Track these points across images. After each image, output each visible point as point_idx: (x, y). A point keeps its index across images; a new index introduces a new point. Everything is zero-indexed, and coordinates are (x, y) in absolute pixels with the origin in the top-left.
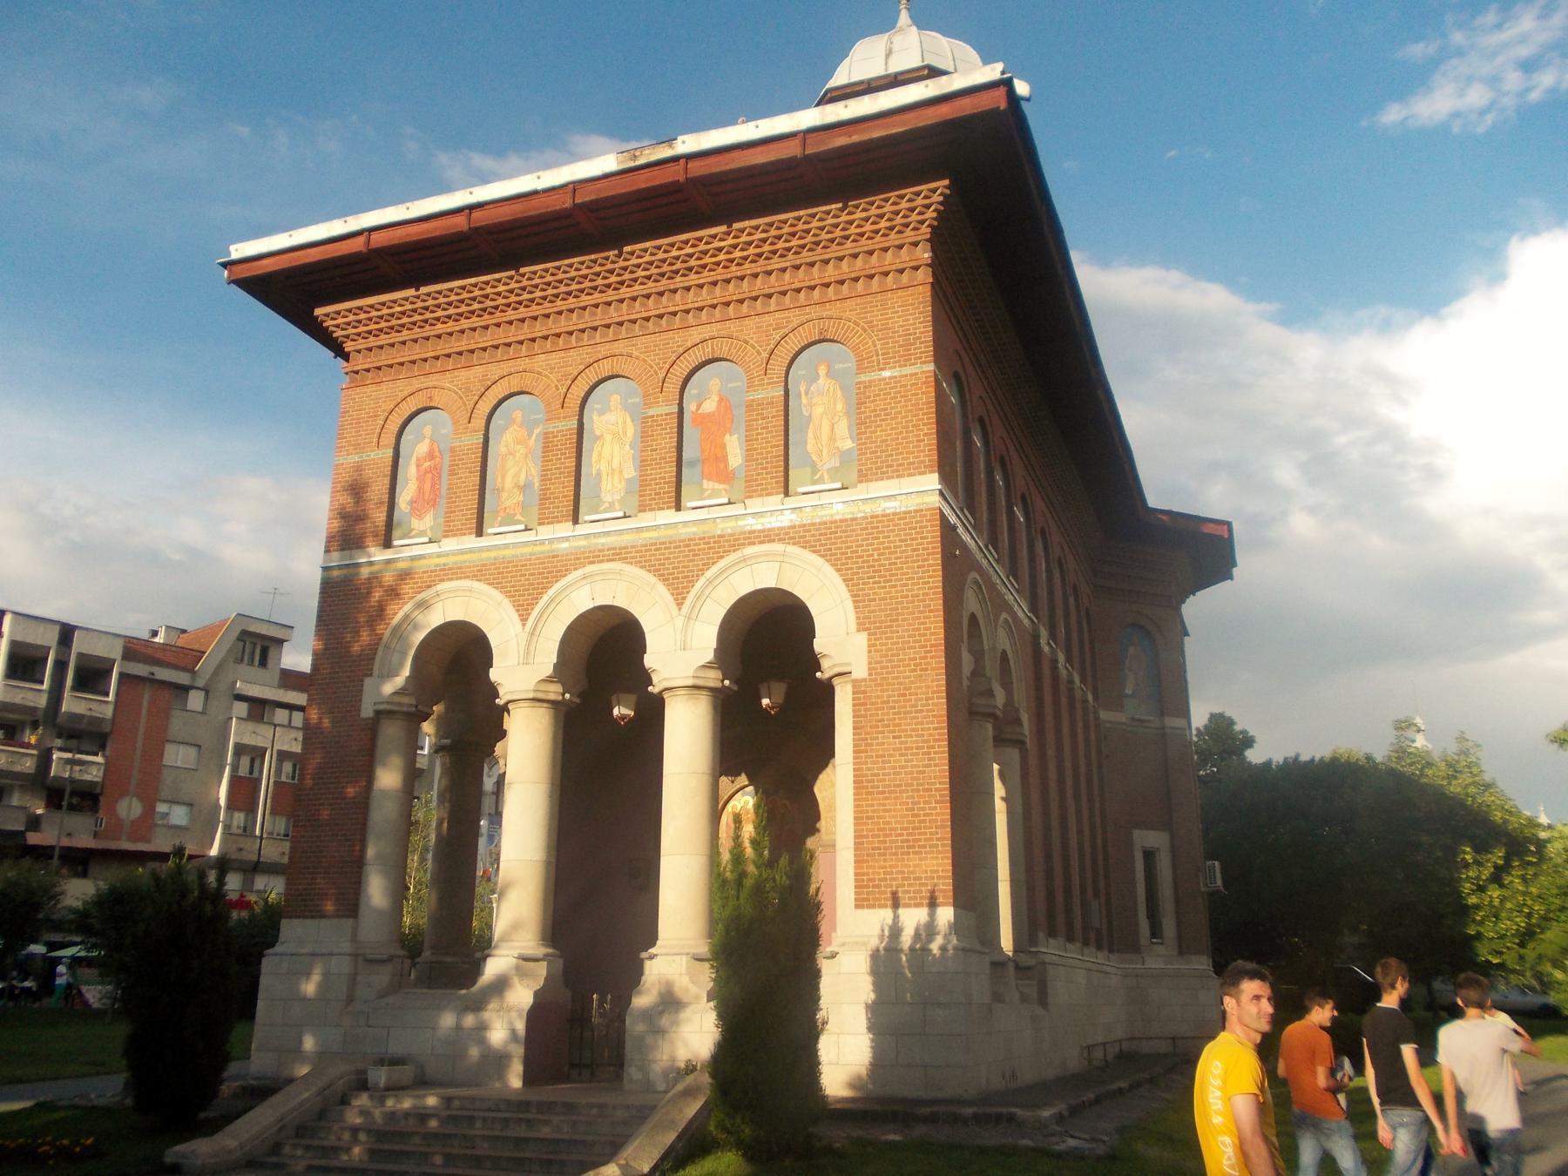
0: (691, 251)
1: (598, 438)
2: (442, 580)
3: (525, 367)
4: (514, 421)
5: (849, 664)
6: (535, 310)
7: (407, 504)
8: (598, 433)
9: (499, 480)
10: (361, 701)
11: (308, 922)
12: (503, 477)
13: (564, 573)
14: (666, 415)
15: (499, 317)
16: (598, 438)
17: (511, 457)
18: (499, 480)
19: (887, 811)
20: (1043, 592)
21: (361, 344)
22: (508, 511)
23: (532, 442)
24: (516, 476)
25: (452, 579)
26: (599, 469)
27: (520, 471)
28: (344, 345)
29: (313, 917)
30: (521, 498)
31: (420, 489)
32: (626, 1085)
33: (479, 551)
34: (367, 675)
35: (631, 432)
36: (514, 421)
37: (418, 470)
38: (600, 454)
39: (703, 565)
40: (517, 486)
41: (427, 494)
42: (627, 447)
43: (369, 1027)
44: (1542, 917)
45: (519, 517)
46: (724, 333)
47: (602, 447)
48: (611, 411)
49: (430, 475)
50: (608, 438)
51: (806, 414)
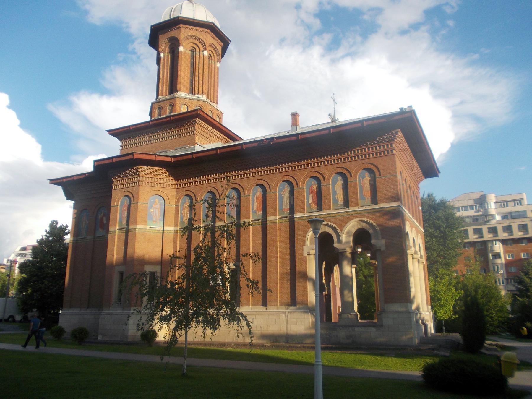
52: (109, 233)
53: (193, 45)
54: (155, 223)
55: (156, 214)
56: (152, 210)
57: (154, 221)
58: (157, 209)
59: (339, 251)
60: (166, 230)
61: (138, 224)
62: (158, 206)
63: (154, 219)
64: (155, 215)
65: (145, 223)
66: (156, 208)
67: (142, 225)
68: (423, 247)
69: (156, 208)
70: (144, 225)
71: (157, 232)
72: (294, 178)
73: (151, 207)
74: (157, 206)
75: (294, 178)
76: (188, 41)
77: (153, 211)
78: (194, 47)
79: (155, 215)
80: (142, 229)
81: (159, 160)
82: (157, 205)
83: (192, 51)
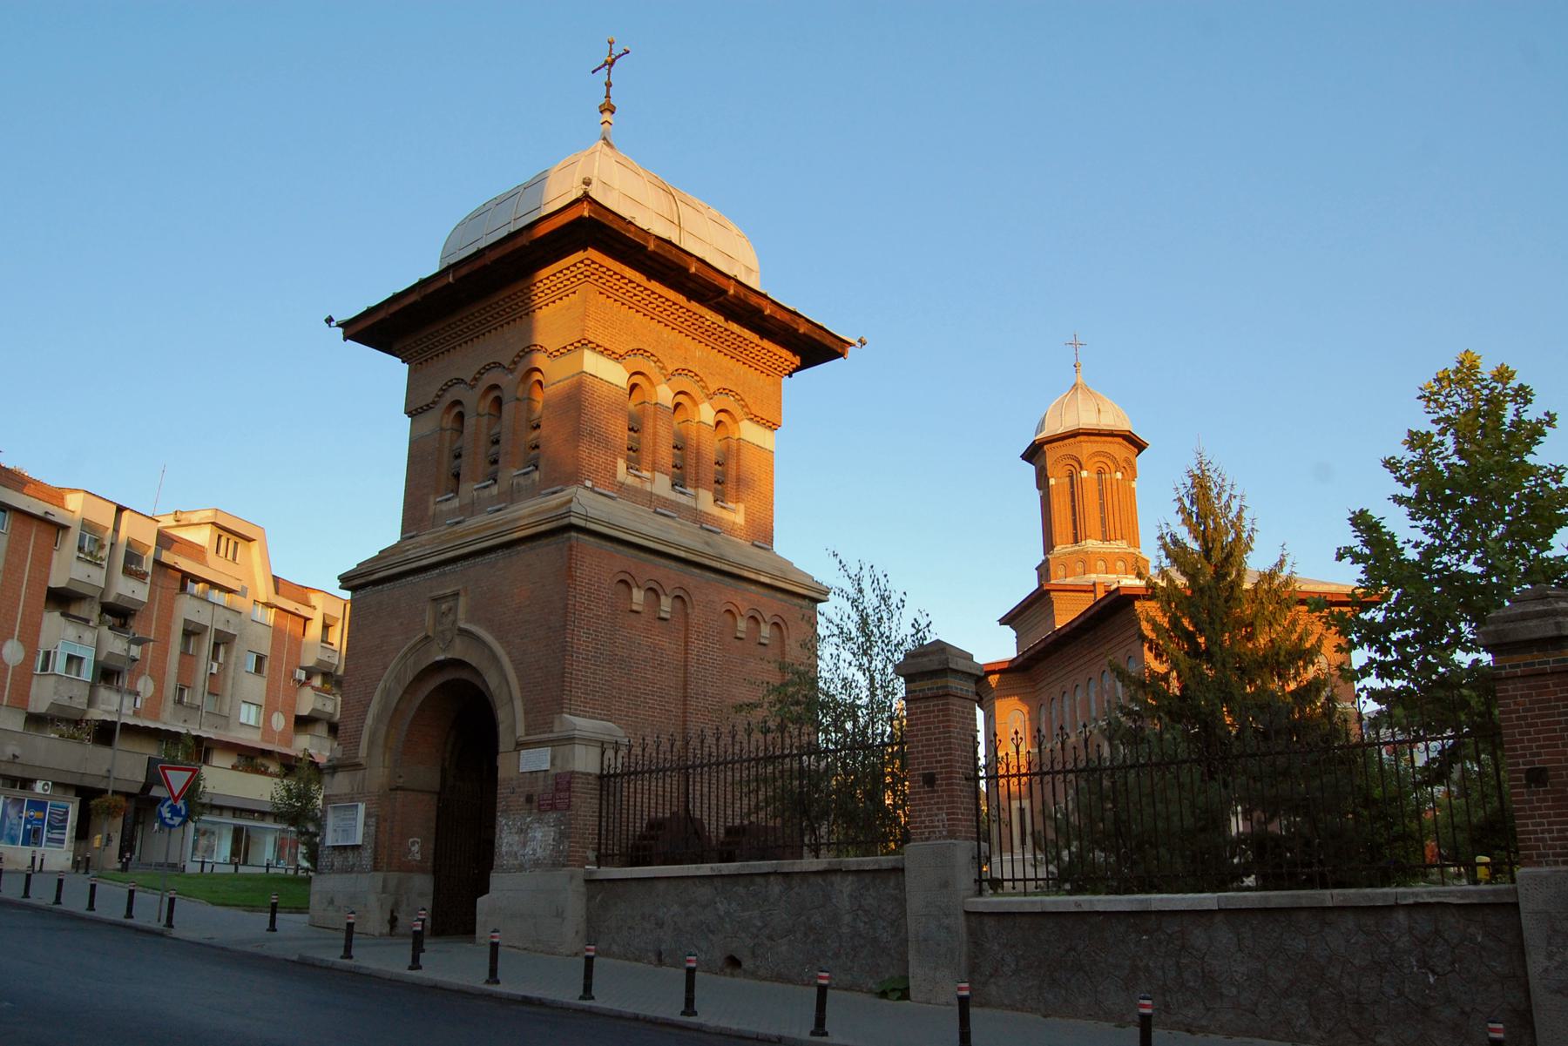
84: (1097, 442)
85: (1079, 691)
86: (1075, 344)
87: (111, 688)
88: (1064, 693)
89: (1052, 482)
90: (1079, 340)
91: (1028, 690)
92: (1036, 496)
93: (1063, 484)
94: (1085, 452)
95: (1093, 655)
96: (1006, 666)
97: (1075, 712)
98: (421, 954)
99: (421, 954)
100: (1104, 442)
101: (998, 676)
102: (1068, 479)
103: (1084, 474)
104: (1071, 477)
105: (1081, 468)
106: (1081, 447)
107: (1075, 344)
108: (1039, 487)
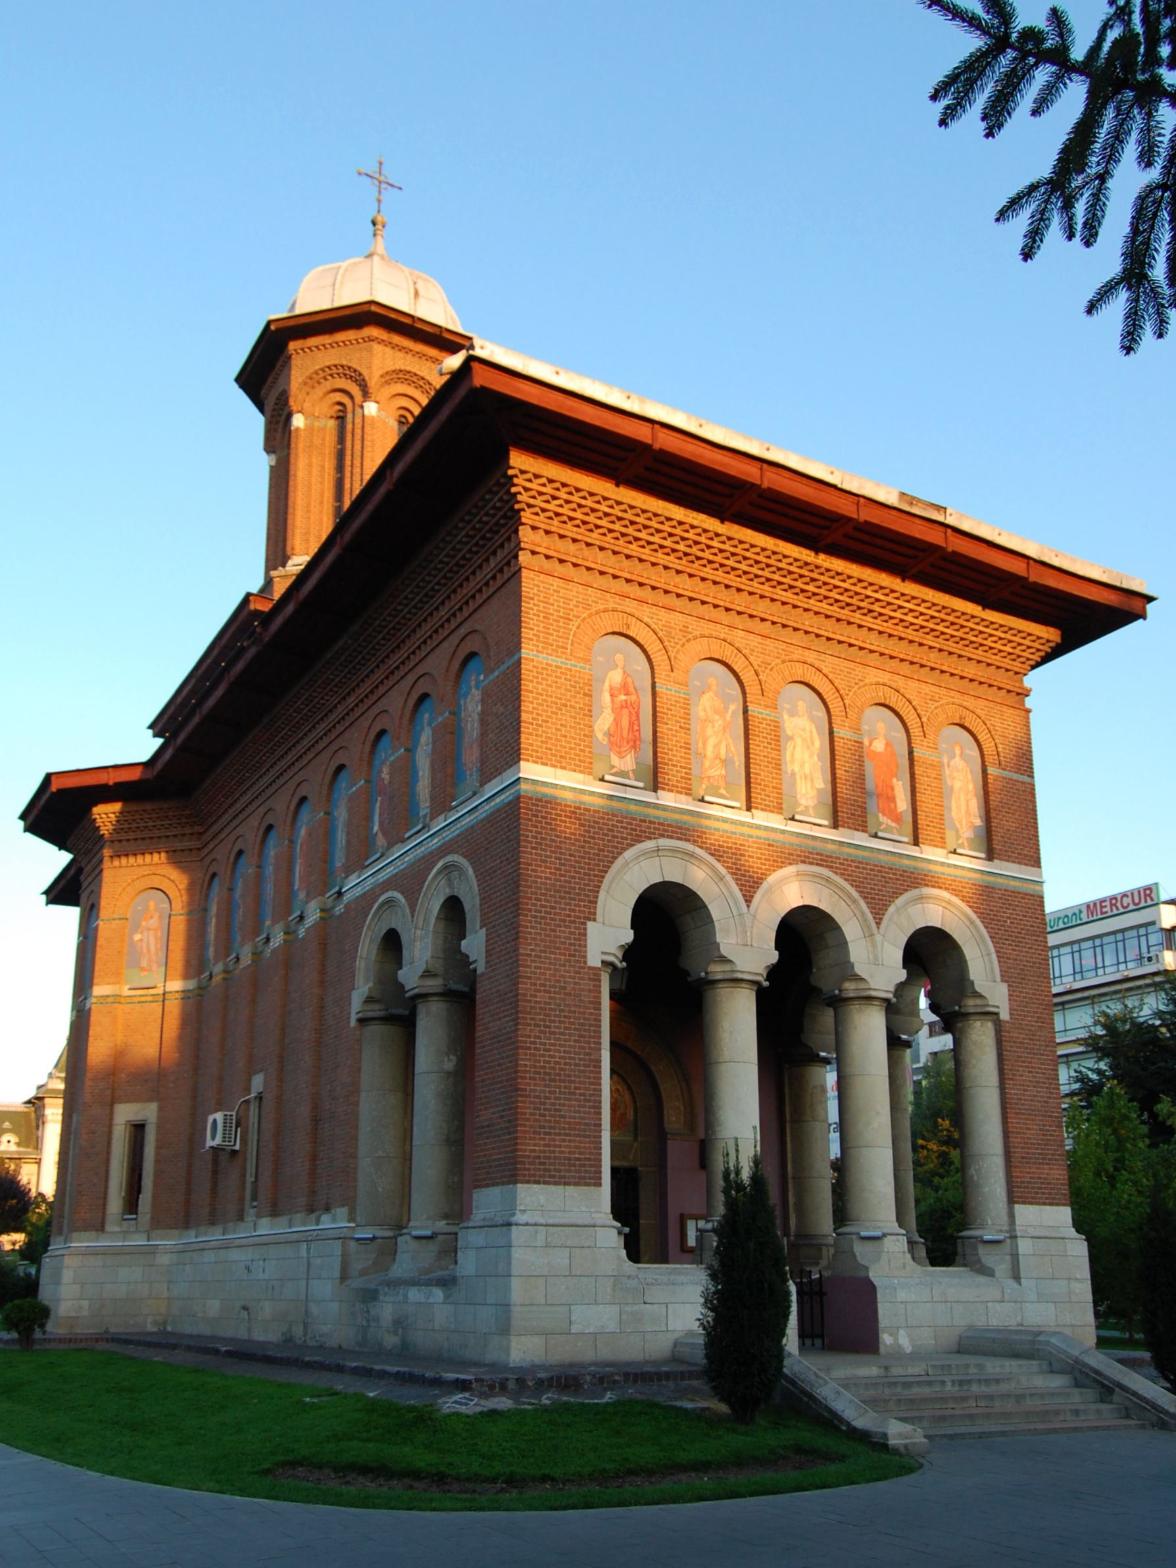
0: (806, 573)
1: (791, 738)
2: (663, 836)
3: (726, 636)
4: (710, 688)
5: (998, 1007)
6: (731, 579)
7: (604, 734)
8: (789, 733)
9: (700, 745)
10: (585, 946)
11: (552, 1188)
12: (704, 744)
13: (780, 864)
14: (855, 741)
15: (695, 568)
16: (791, 738)
17: (710, 725)
18: (700, 745)
19: (1029, 1129)
20: (93, 875)
21: (541, 521)
22: (712, 781)
23: (728, 716)
24: (716, 746)
25: (672, 837)
26: (793, 770)
27: (720, 742)
28: (522, 513)
29: (556, 1183)
30: (723, 772)
31: (616, 722)
32: (882, 1349)
33: (731, 823)
34: (589, 919)
35: (817, 744)
36: (710, 688)
37: (613, 701)
38: (793, 755)
39: (893, 893)
40: (717, 757)
41: (625, 732)
42: (815, 758)
43: (645, 1303)
44: (509, 1224)
45: (723, 791)
46: (894, 685)
47: (794, 748)
48: (799, 716)
49: (625, 711)
50: (799, 741)
51: (950, 784)
52: (477, 1040)
53: (339, 397)
54: (145, 973)
55: (148, 946)
56: (137, 937)
57: (143, 969)
58: (151, 932)
59: (623, 988)
60: (171, 992)
61: (98, 984)
62: (154, 922)
63: (144, 964)
64: (145, 951)
65: (117, 977)
66: (149, 929)
67: (108, 984)
68: (294, 503)
69: (149, 929)
70: (114, 983)
71: (151, 1002)
72: (744, 693)
73: (136, 928)
74: (151, 921)
75: (744, 693)
76: (319, 391)
77: (141, 940)
78: (339, 403)
79: (145, 951)
80: (108, 996)
81: (117, 780)
82: (151, 917)
83: (338, 418)
84: (402, 349)
85: (305, 815)
86: (381, 182)
87: (56, 1066)
88: (270, 828)
89: (298, 421)
90: (390, 174)
91: (186, 844)
92: (263, 463)
93: (324, 429)
94: (376, 362)
95: (351, 700)
96: (135, 775)
97: (291, 870)
98: (590, 924)
99: (590, 924)
100: (422, 355)
101: (117, 807)
102: (332, 424)
103: (371, 408)
104: (341, 418)
105: (366, 395)
106: (370, 350)
107: (381, 182)
108: (269, 448)
